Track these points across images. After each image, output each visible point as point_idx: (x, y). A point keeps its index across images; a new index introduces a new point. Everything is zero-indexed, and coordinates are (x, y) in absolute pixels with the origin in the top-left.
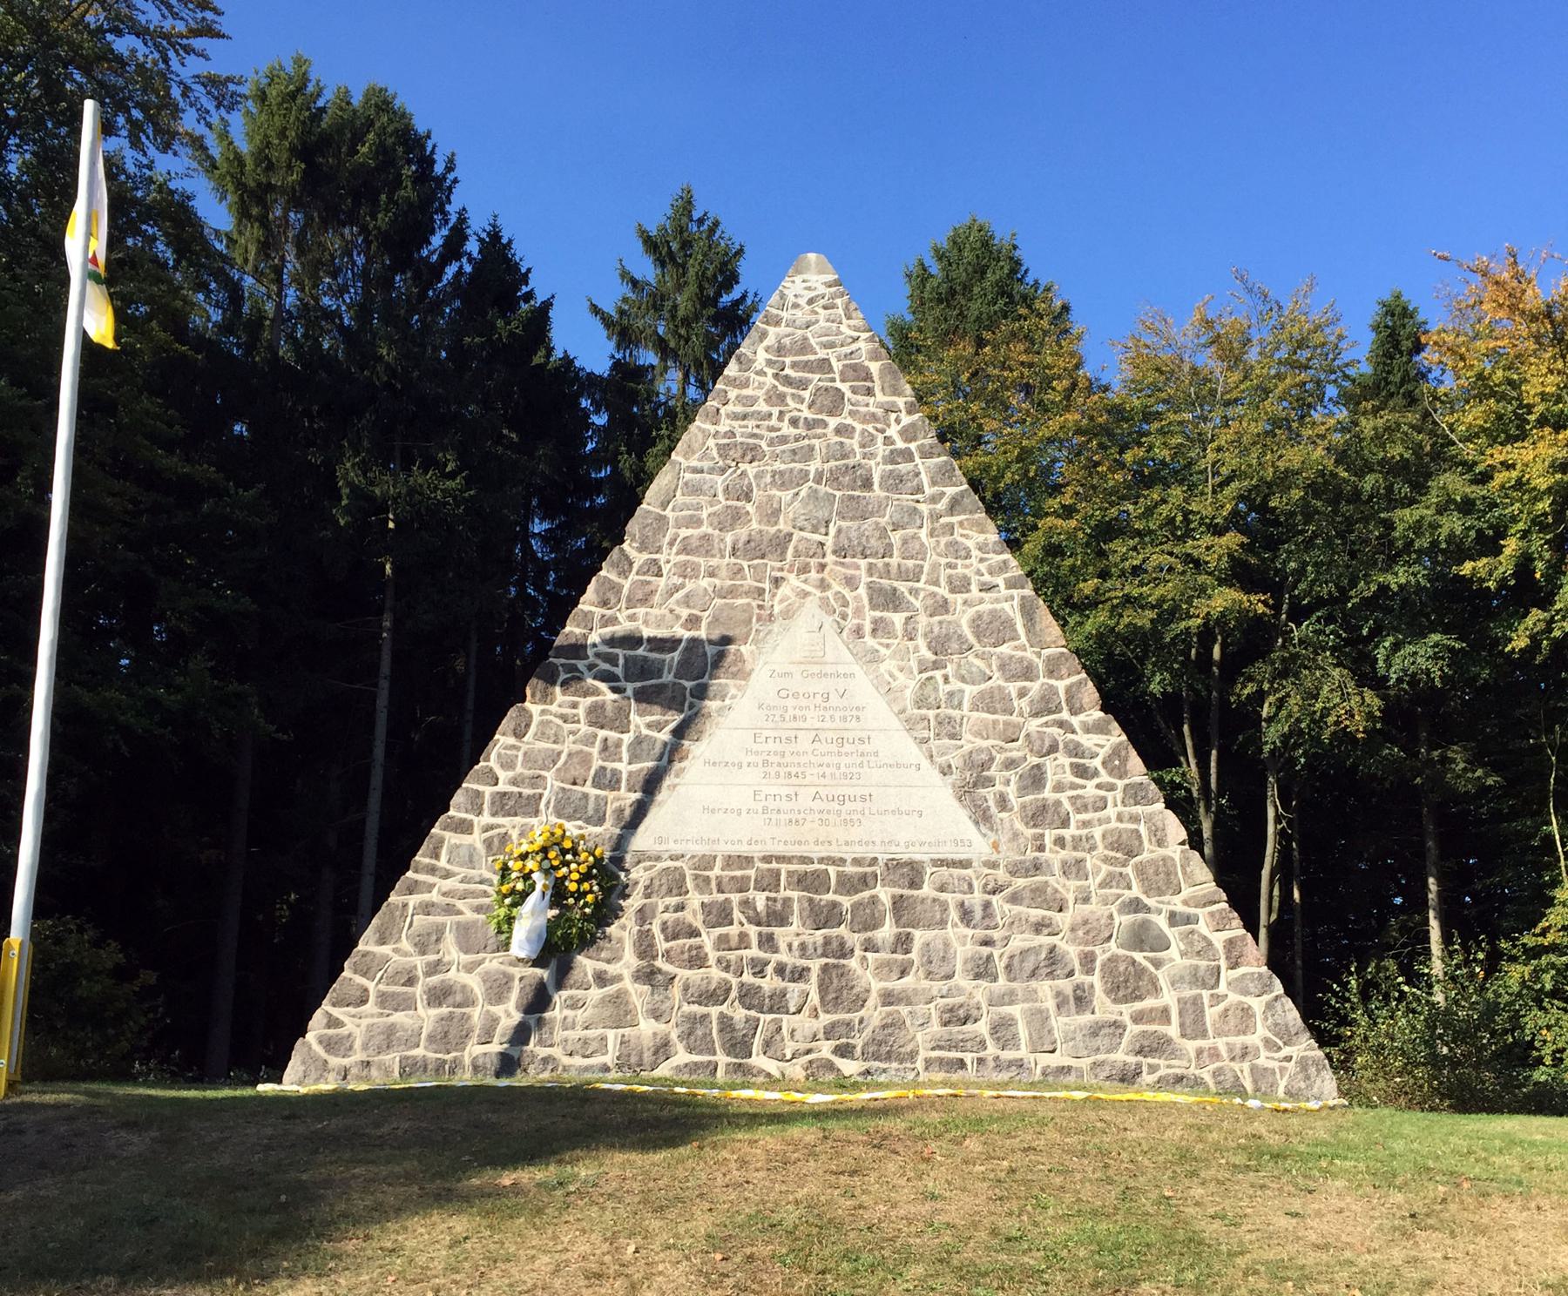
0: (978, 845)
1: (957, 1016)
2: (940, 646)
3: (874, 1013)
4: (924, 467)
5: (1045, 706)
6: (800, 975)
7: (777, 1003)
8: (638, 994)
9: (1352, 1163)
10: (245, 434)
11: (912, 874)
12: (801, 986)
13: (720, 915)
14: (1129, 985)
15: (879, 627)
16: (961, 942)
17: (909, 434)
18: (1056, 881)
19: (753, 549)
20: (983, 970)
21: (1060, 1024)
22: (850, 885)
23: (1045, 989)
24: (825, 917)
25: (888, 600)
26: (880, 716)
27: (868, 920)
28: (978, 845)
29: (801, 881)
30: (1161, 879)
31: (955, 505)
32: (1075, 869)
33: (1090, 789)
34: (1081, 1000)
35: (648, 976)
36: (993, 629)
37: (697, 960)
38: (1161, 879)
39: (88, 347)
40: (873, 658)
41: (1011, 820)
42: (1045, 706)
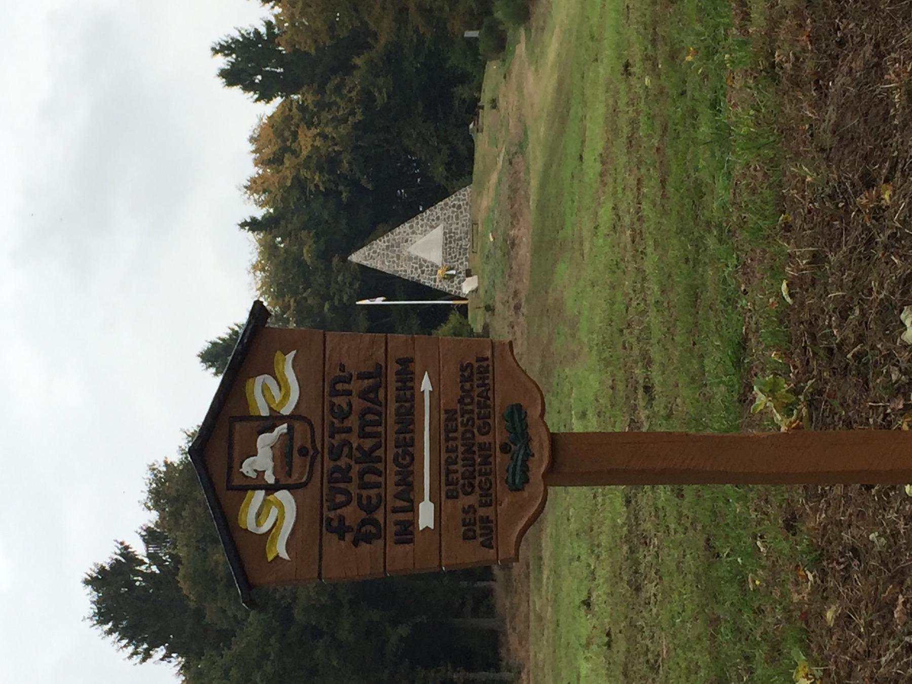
0: (441, 226)
1: (463, 226)
2: (413, 233)
3: (463, 235)
4: (386, 239)
5: (422, 220)
6: (458, 244)
7: (461, 246)
8: (460, 261)
9: (652, 312)
10: (280, 549)
11: (445, 233)
12: (490, 466)
13: (450, 254)
14: (459, 207)
15: (411, 241)
16: (454, 226)
17: (380, 241)
18: (446, 216)
19: (398, 259)
20: (458, 224)
21: (464, 214)
22: (446, 239)
23: (460, 216)
24: (450, 242)
25: (406, 241)
26: (424, 239)
27: (450, 237)
28: (441, 226)
29: (446, 244)
30: (446, 204)
31: (392, 234)
32: (445, 214)
33: (434, 213)
34: (461, 213)
35: (457, 261)
36: (411, 227)
37: (456, 256)
38: (446, 204)
39: (384, 301)
40: (415, 242)
41: (438, 222)
42: (422, 220)
